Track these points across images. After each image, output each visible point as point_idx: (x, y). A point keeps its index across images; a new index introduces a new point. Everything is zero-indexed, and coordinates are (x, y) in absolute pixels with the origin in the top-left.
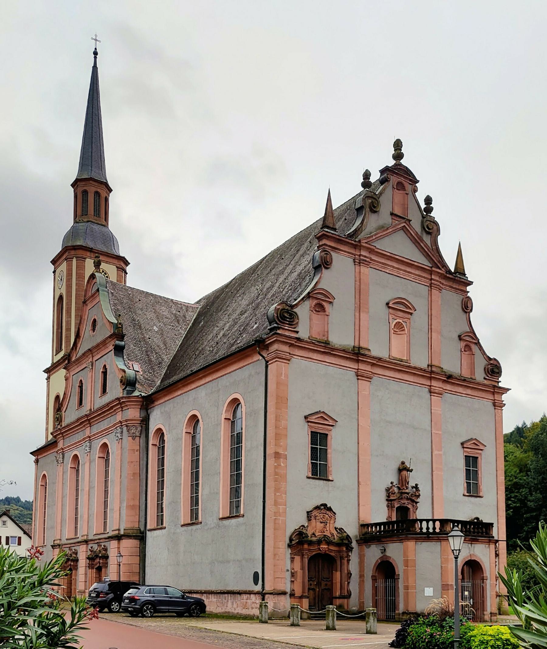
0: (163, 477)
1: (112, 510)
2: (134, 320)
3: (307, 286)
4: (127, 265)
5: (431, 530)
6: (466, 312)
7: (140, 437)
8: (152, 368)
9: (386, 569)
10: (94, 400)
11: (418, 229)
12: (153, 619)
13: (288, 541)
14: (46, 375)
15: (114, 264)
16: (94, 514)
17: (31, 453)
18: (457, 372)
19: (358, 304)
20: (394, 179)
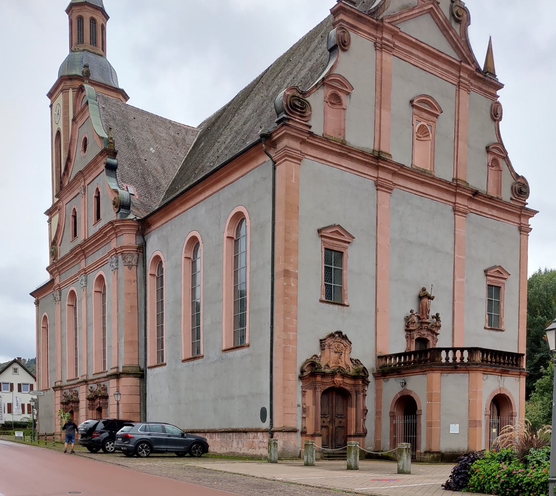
1: (110, 347)
2: (128, 139)
5: (458, 361)
6: (495, 120)
8: (149, 192)
9: (407, 405)
10: (88, 228)
11: (447, 14)
12: (149, 459)
13: (298, 373)
14: (47, 218)
17: (31, 294)
18: (482, 190)
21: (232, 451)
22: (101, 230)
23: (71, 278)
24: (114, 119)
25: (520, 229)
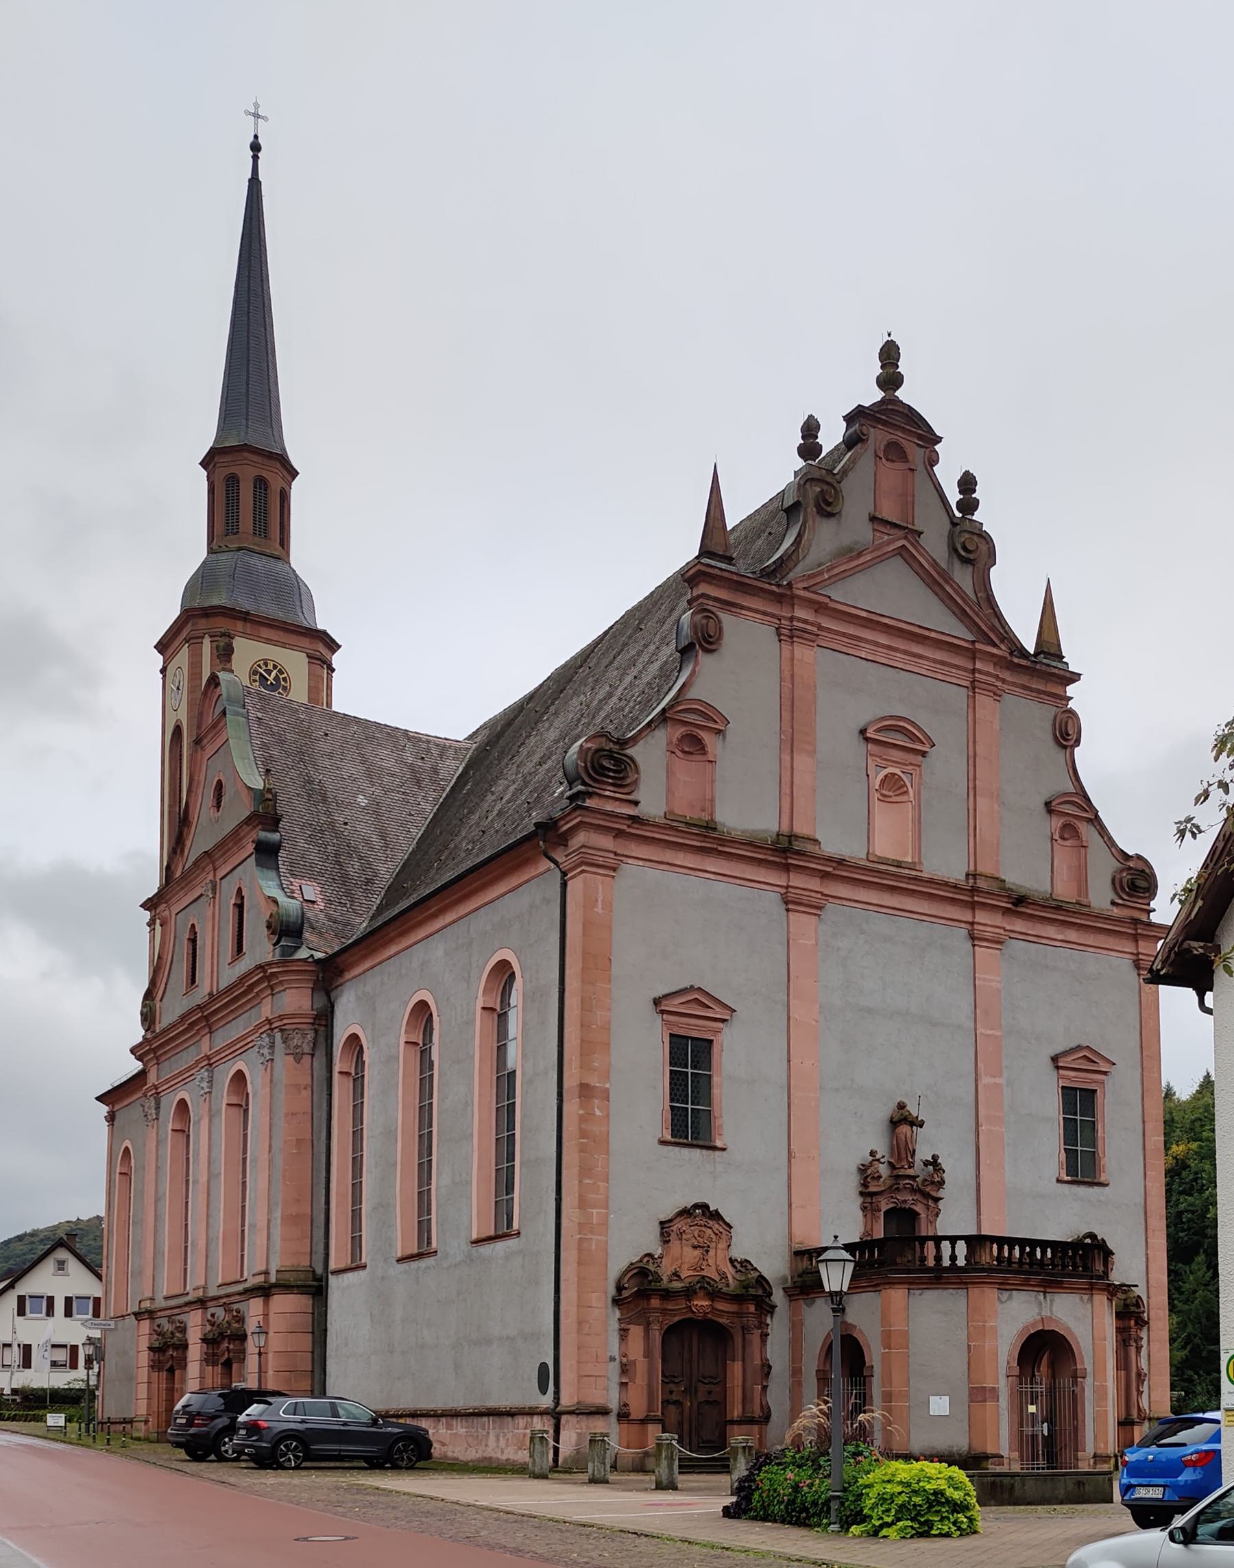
1: (253, 1226)
2: (310, 782)
4: (334, 652)
5: (946, 1262)
6: (1065, 747)
7: (313, 1055)
8: (348, 893)
9: (850, 1357)
10: (219, 971)
13: (612, 1291)
15: (299, 649)
16: (218, 1238)
17: (97, 1099)
18: (1042, 889)
20: (878, 437)
21: (486, 1455)
22: (242, 979)
23: (181, 1073)
24: (281, 742)
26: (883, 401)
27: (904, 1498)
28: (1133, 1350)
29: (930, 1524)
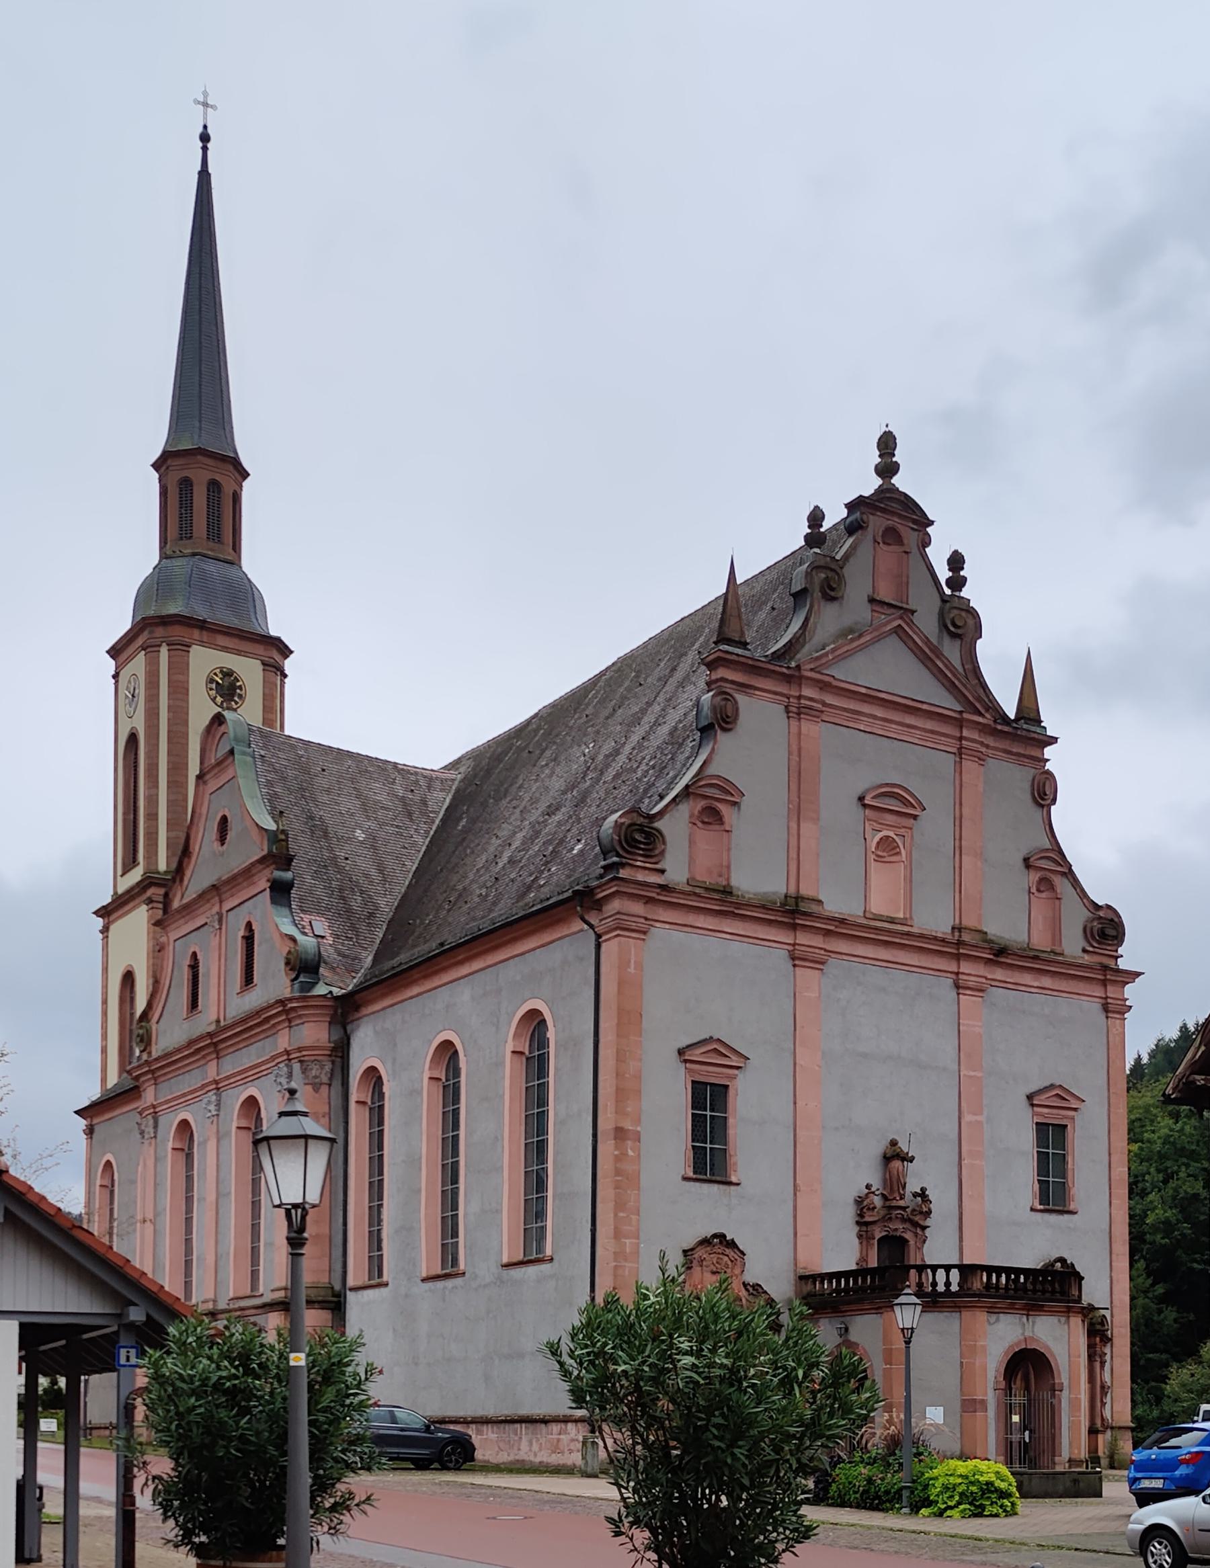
0: (381, 1173)
1: (270, 1244)
2: (312, 818)
3: (686, 766)
4: (286, 657)
5: (941, 1288)
6: (1042, 806)
7: (330, 1085)
8: (353, 927)
10: (224, 1000)
14: (100, 922)
15: (254, 656)
16: (228, 1254)
19: (796, 804)
20: (877, 523)
23: (184, 1095)
24: (284, 779)
25: (1106, 1009)
26: (879, 491)
27: (963, 1487)
28: (1098, 1365)
29: (983, 1507)
